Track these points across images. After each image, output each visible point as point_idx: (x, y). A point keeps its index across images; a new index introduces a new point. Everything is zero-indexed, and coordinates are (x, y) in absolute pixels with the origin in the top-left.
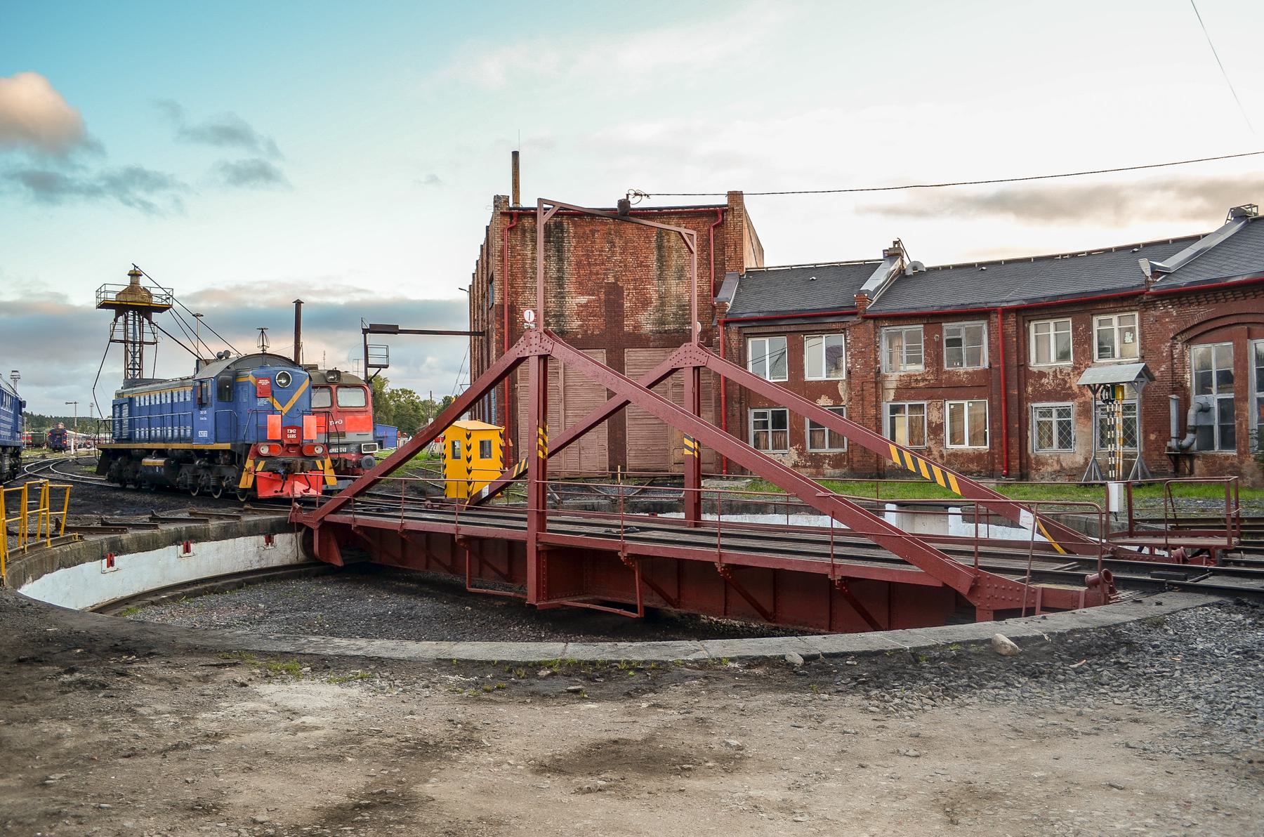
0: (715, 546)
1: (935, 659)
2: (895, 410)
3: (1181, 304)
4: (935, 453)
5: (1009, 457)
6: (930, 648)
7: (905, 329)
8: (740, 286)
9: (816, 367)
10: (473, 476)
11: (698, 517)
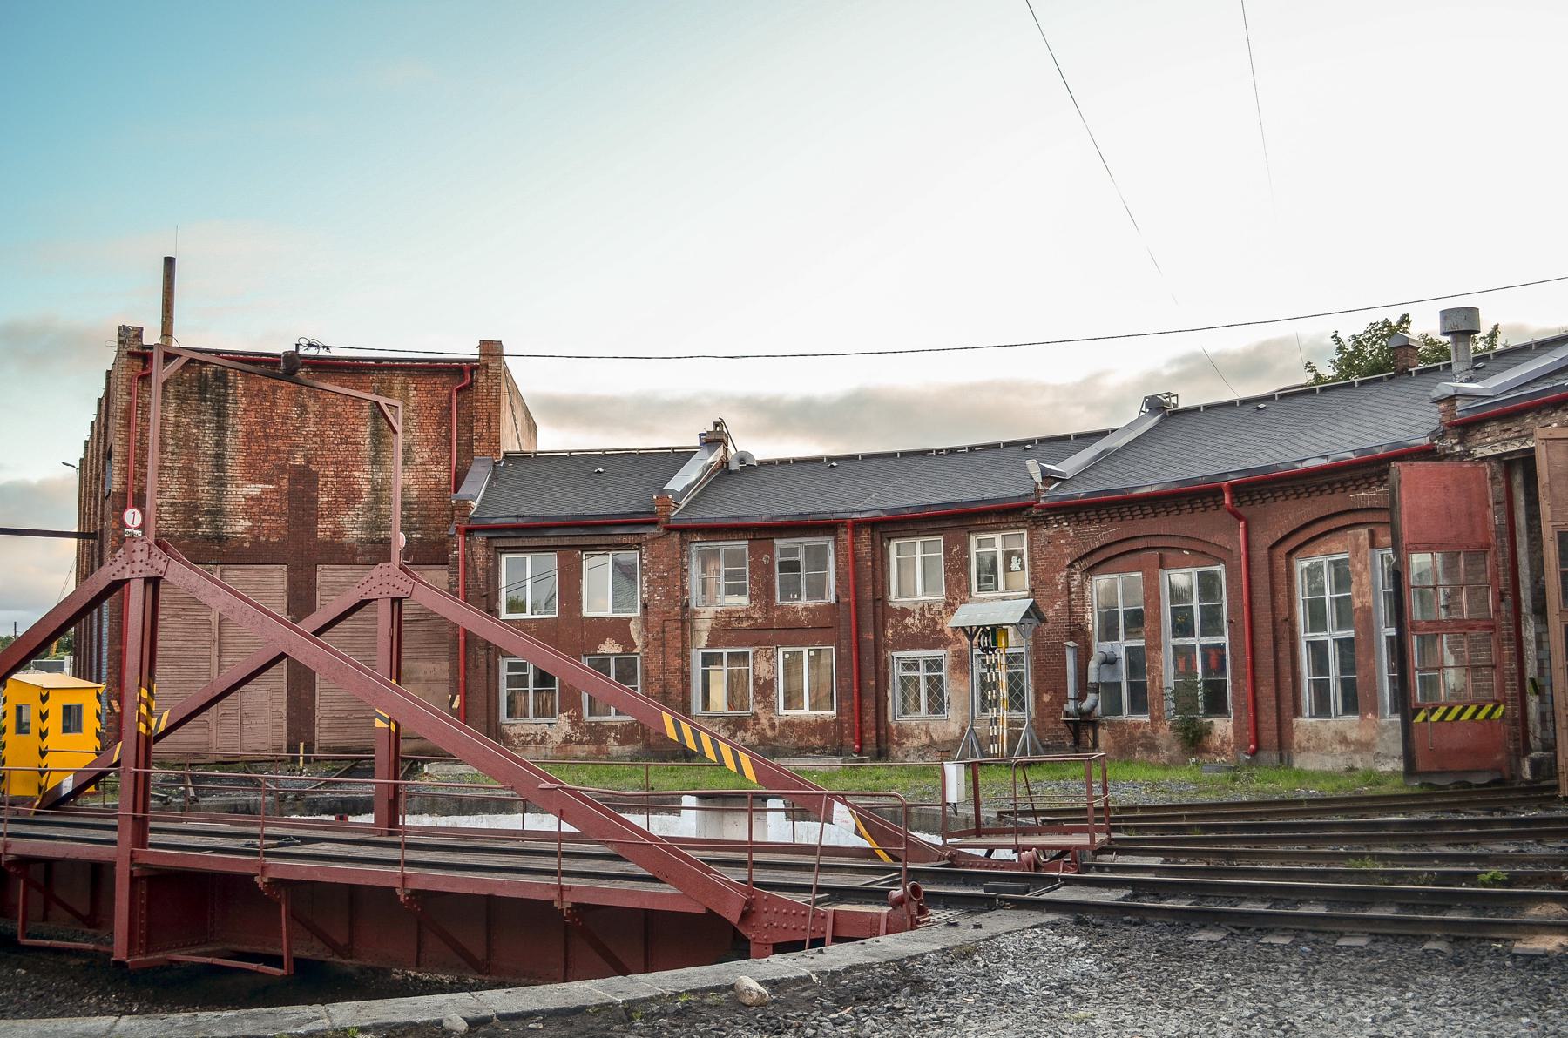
0: (396, 863)
1: (653, 1015)
2: (708, 660)
3: (1080, 521)
4: (764, 721)
5: (863, 731)
6: (652, 999)
7: (724, 546)
8: (494, 477)
10: (50, 761)
11: (393, 821)
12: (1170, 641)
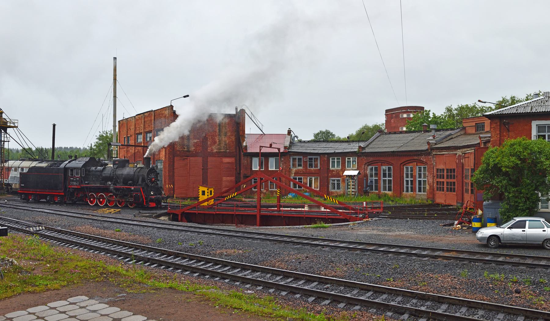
9: (412, 116)
12: (382, 178)
